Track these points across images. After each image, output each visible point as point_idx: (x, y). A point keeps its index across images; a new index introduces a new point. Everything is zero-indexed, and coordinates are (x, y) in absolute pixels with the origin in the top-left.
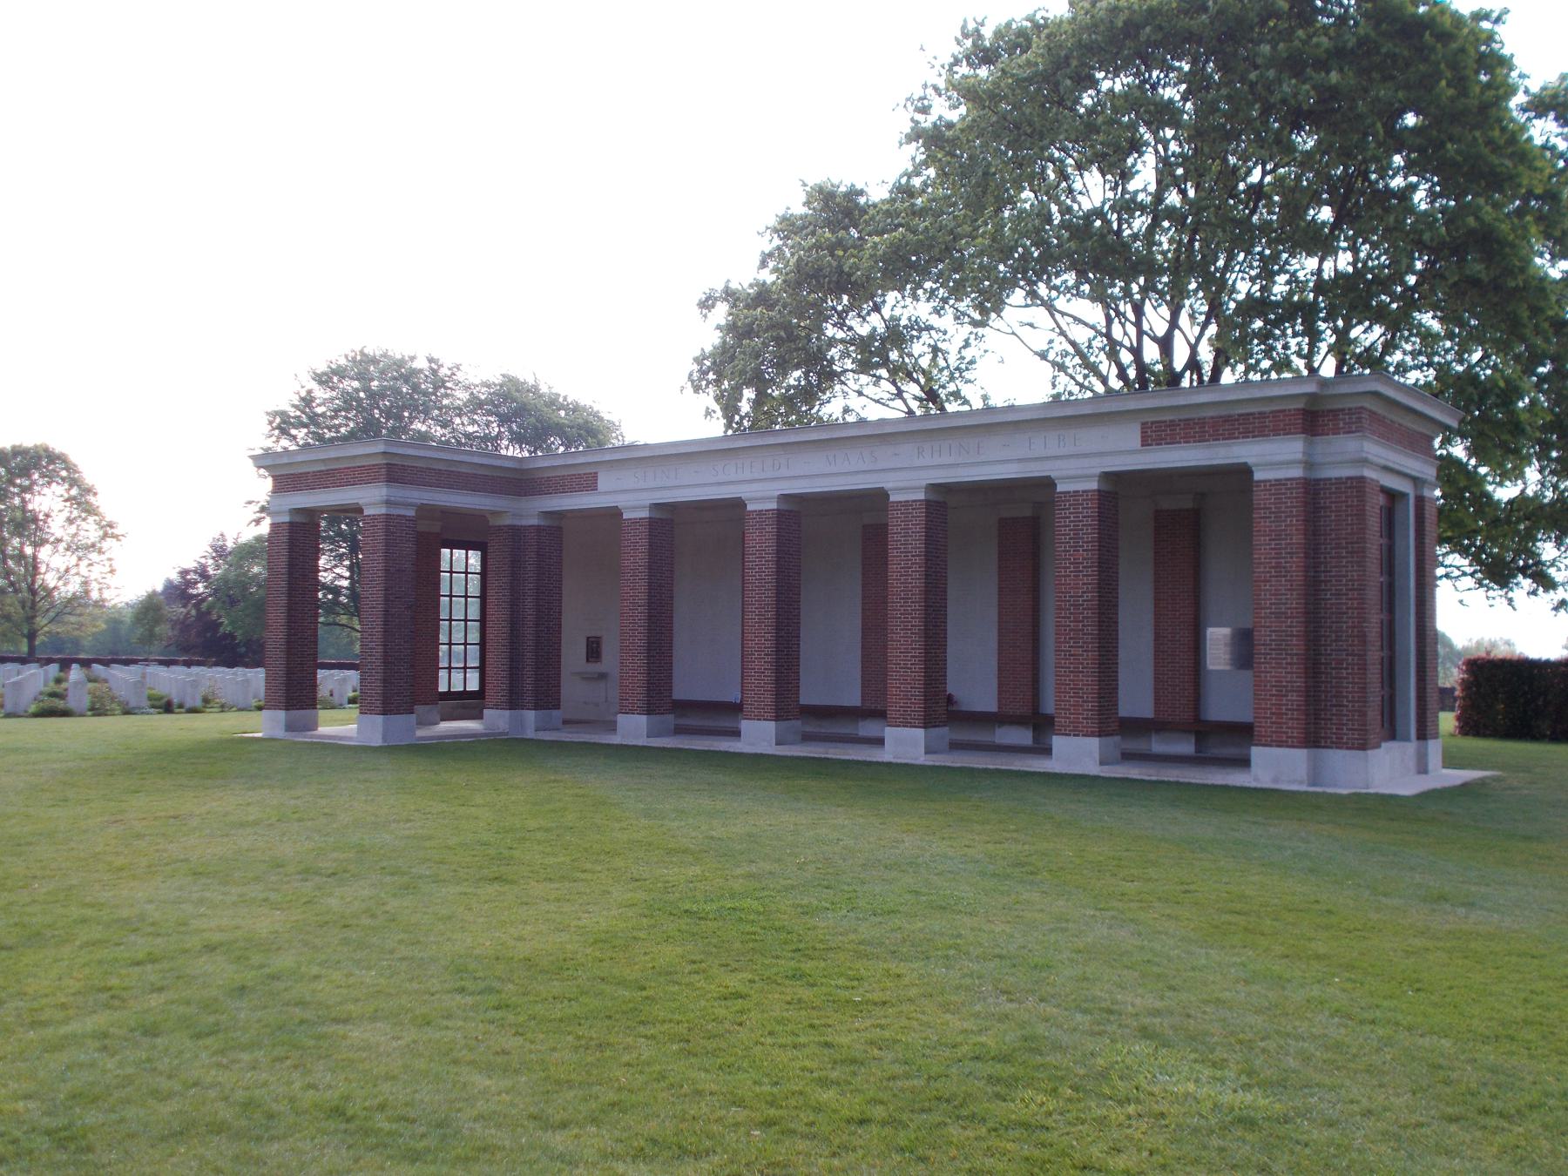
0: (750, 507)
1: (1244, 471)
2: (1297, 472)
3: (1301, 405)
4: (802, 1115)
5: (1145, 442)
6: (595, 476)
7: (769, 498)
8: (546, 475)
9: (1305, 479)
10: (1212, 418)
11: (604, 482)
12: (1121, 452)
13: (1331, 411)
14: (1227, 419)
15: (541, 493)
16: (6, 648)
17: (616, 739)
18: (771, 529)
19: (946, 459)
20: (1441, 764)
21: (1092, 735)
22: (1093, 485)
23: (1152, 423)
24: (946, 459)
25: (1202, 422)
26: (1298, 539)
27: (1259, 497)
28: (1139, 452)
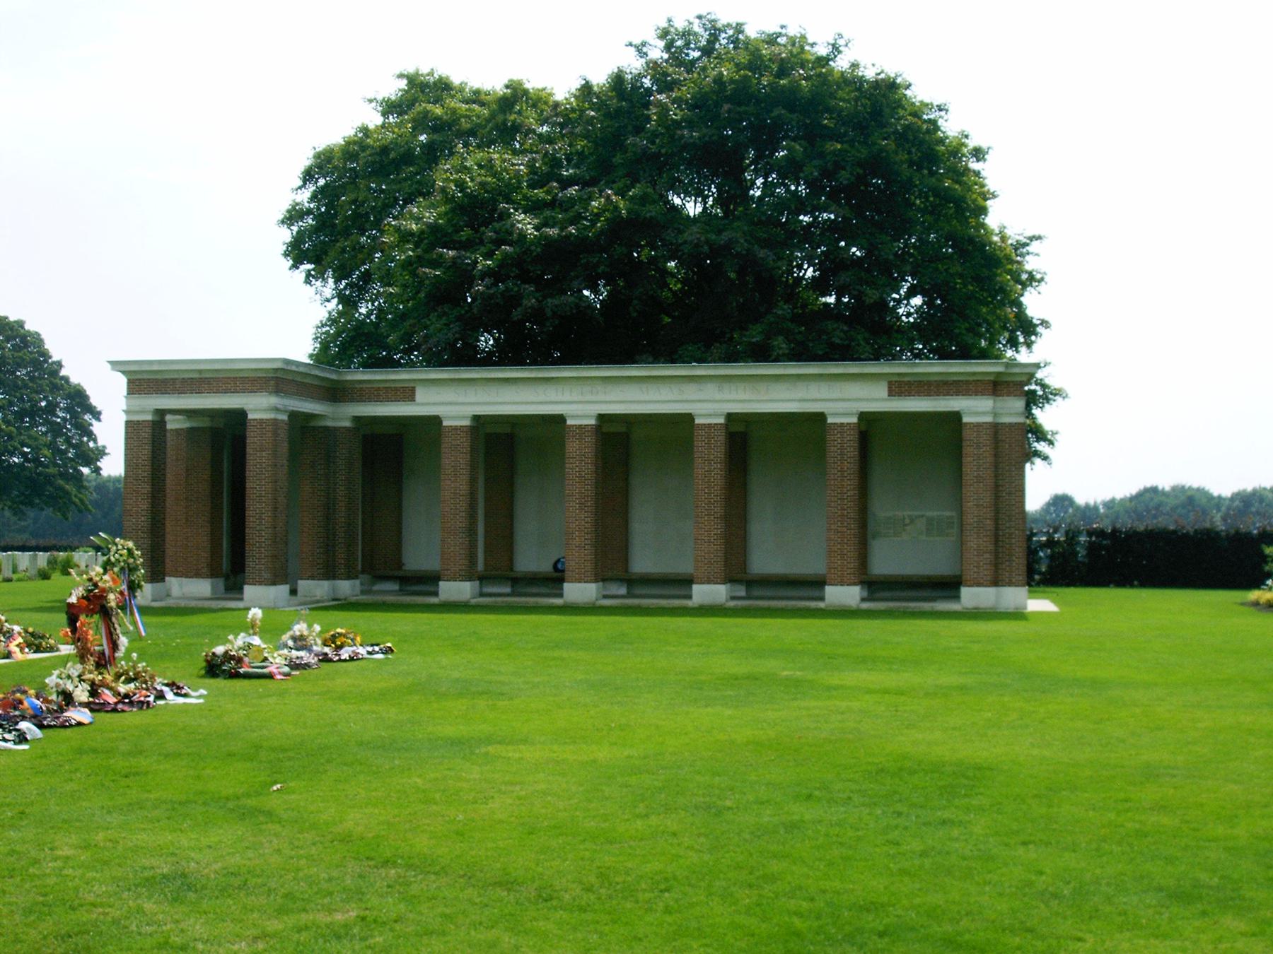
0: (569, 422)
1: (956, 417)
2: (989, 419)
3: (992, 378)
4: (285, 845)
5: (892, 393)
6: (413, 390)
7: (464, 417)
8: (1005, 379)
9: (211, 428)
10: (936, 381)
11: (421, 394)
12: (533, 403)
13: (1006, 382)
14: (946, 383)
15: (352, 400)
16: (8, 540)
17: (821, 605)
18: (590, 439)
19: (742, 396)
20: (162, 584)
21: (854, 584)
22: (593, 422)
23: (896, 382)
24: (742, 396)
25: (929, 384)
26: (990, 459)
27: (966, 433)
28: (886, 400)
